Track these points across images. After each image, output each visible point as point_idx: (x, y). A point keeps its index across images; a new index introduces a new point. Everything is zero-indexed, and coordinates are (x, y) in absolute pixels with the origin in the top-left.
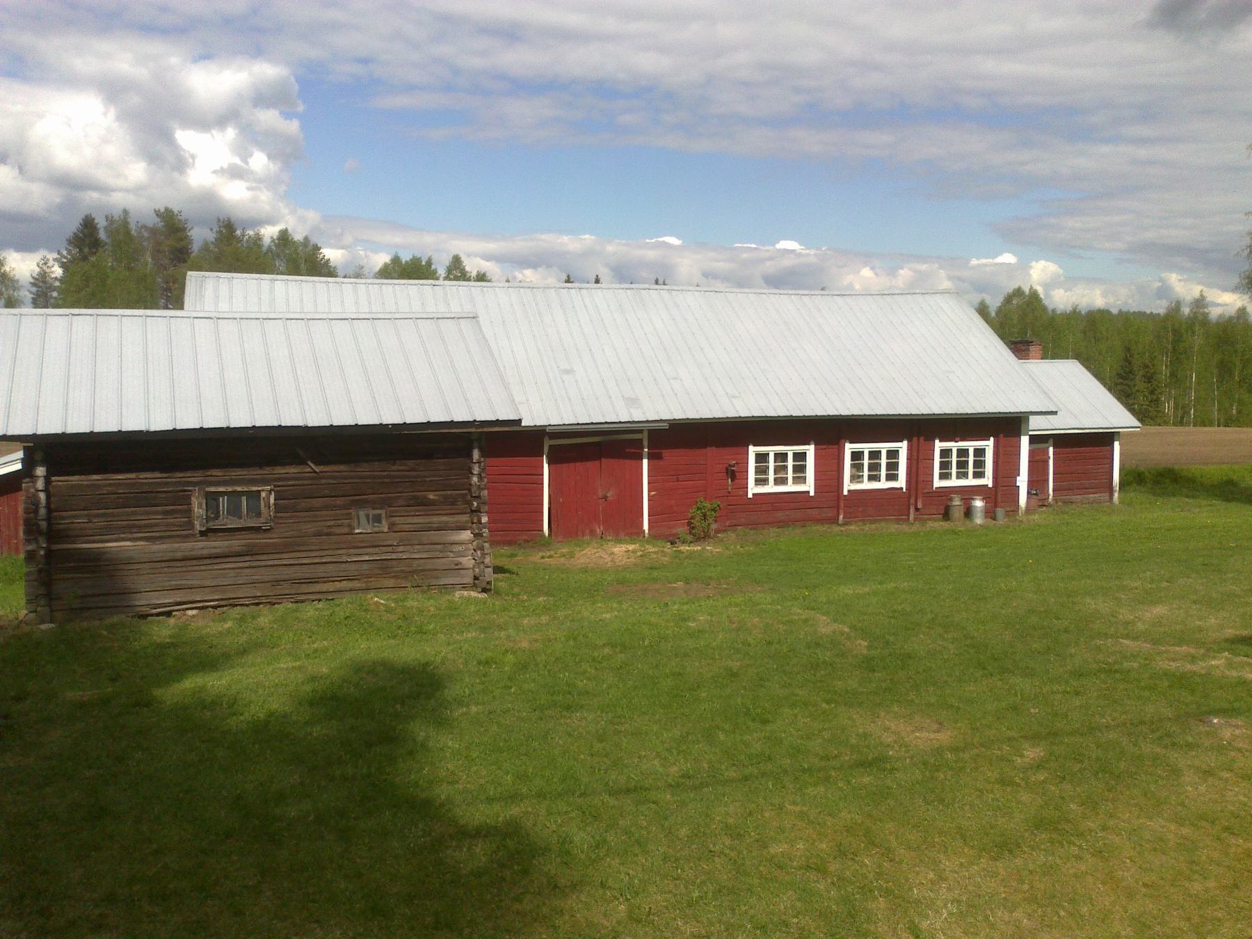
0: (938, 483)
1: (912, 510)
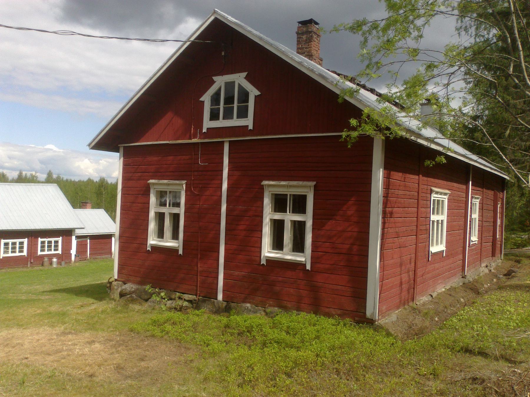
0: (39, 253)
1: (29, 263)
